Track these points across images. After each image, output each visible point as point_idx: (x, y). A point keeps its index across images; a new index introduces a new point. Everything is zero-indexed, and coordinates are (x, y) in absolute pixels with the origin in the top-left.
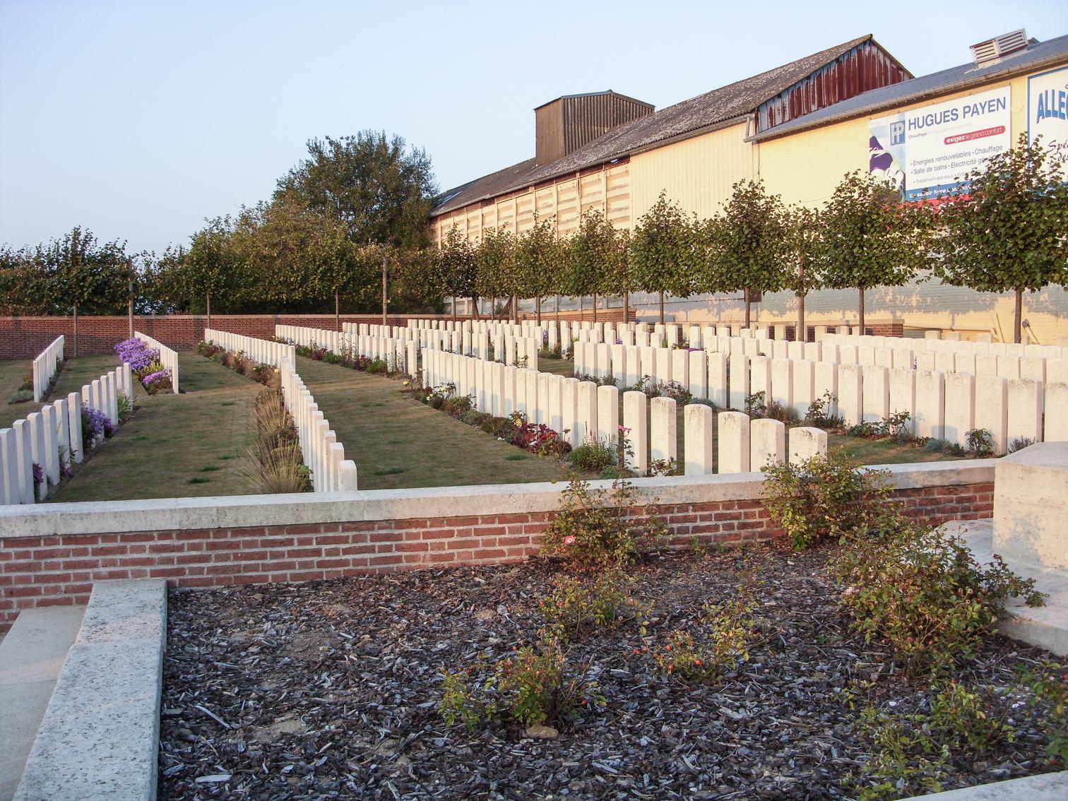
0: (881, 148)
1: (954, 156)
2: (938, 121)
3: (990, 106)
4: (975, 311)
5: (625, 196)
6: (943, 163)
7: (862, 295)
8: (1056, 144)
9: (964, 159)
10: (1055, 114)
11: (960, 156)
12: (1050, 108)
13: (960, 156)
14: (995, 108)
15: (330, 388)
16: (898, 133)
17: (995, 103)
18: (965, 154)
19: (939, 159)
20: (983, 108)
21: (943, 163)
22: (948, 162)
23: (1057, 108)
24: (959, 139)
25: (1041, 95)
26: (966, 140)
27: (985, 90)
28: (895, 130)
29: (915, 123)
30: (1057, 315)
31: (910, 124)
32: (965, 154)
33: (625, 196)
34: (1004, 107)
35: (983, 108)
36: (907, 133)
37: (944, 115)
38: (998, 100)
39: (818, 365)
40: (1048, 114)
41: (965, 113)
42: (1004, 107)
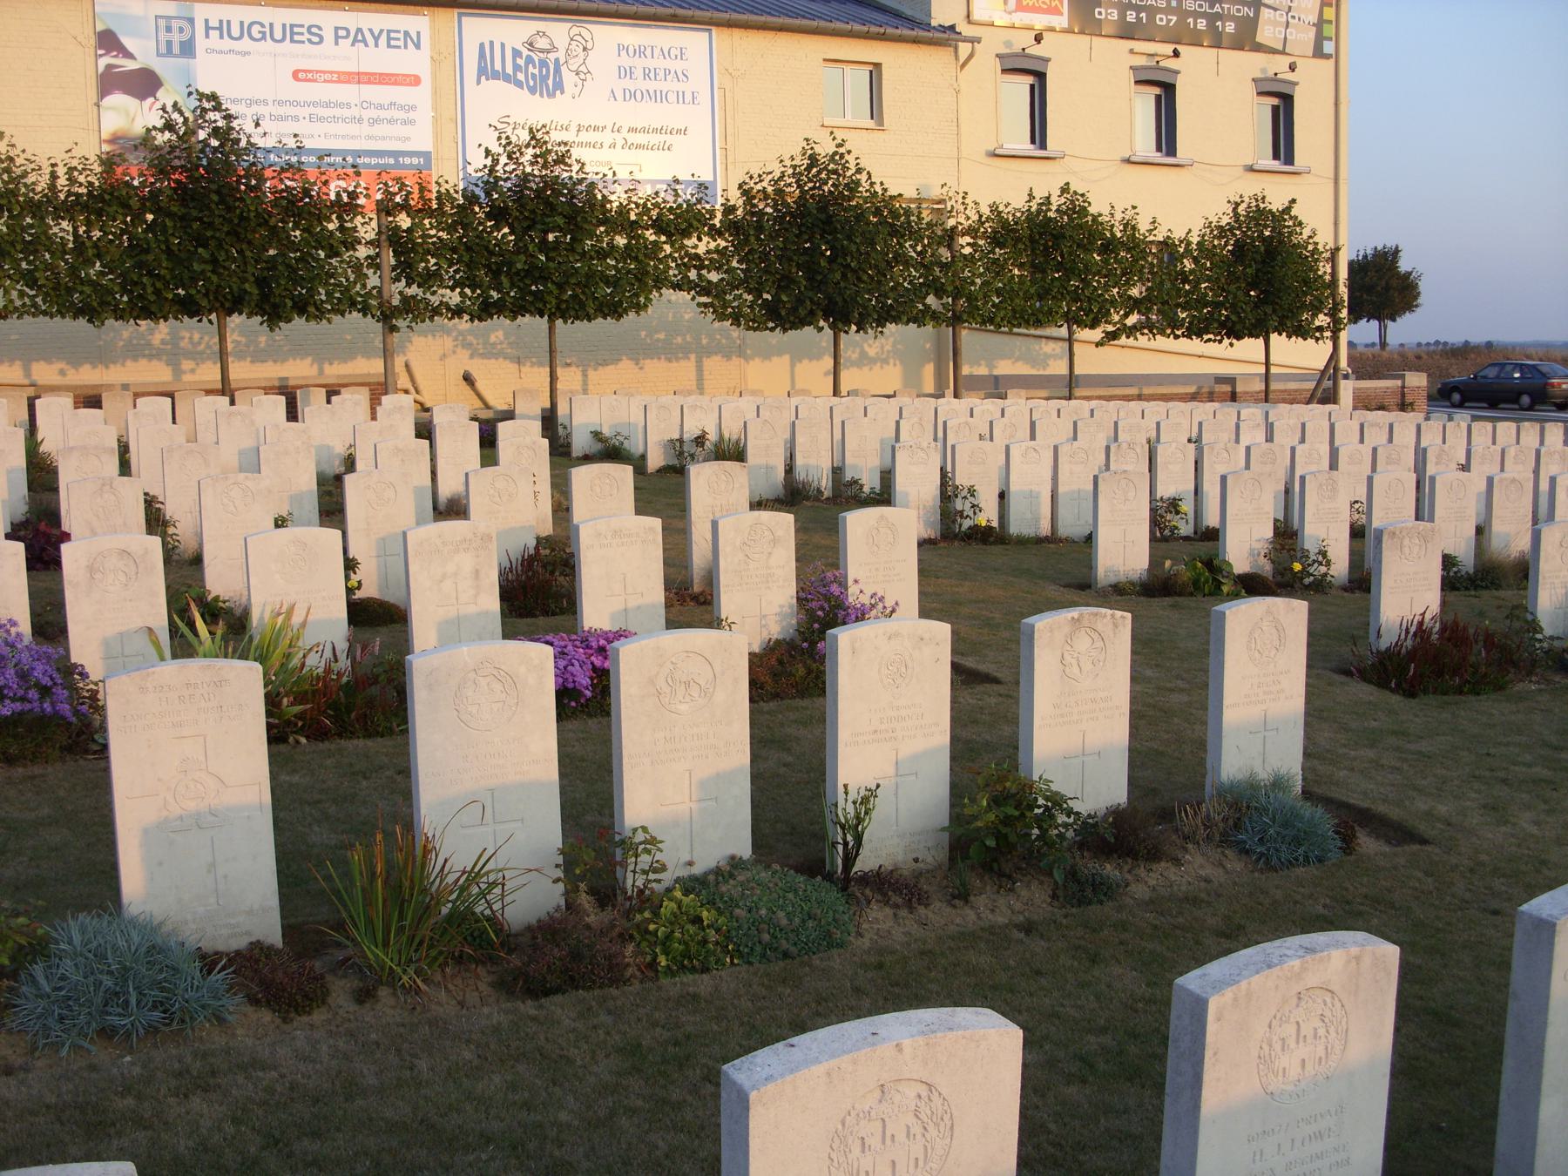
0: (129, 55)
1: (314, 104)
2: (278, 35)
3: (389, 39)
4: (811, 360)
5: (492, 43)
6: (291, 111)
7: (551, 329)
8: (511, 120)
9: (337, 112)
10: (507, 78)
11: (327, 105)
12: (498, 66)
13: (327, 105)
14: (401, 43)
15: (1411, 959)
16: (176, 38)
17: (401, 36)
18: (340, 105)
19: (280, 103)
20: (376, 39)
21: (291, 111)
22: (306, 112)
23: (509, 70)
24: (326, 77)
25: (482, 46)
26: (339, 82)
27: (403, 13)
28: (169, 29)
29: (223, 29)
30: (519, 361)
31: (208, 28)
32: (340, 105)
33: (492, 43)
34: (418, 46)
35: (376, 39)
36: (201, 43)
37: (246, 30)
38: (406, 34)
39: (1300, 449)
40: (495, 76)
41: (337, 37)
42: (418, 46)
